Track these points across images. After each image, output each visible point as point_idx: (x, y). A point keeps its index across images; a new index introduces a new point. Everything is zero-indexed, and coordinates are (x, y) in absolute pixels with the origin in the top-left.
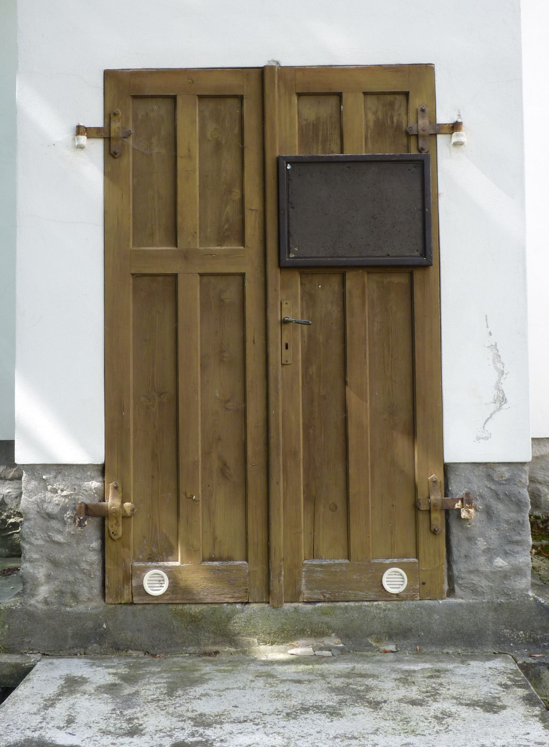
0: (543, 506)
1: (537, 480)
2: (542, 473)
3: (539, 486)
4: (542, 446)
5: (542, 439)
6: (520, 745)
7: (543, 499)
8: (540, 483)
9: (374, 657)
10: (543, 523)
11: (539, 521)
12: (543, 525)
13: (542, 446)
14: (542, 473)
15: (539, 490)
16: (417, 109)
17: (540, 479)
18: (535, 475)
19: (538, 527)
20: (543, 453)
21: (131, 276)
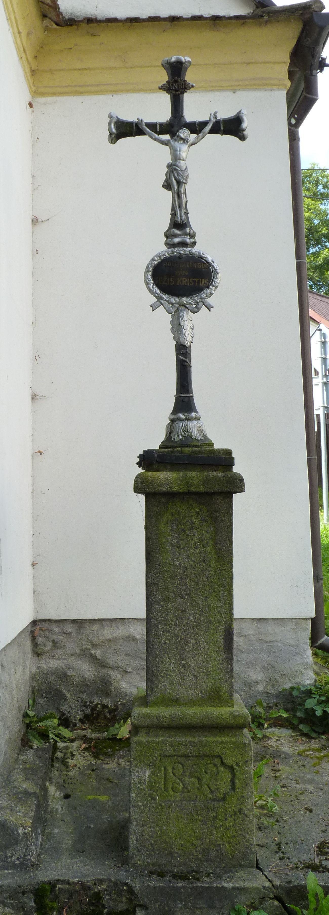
0: (114, 693)
1: (109, 665)
2: (115, 657)
3: (111, 672)
4: (114, 628)
5: (115, 619)
6: (43, 894)
7: (113, 686)
8: (112, 668)
9: (319, 897)
10: (110, 712)
11: (106, 711)
12: (110, 715)
13: (114, 628)
14: (115, 657)
15: (110, 677)
16: (189, 146)
17: (112, 663)
18: (107, 660)
19: (105, 717)
20: (115, 635)
21: (213, 305)
